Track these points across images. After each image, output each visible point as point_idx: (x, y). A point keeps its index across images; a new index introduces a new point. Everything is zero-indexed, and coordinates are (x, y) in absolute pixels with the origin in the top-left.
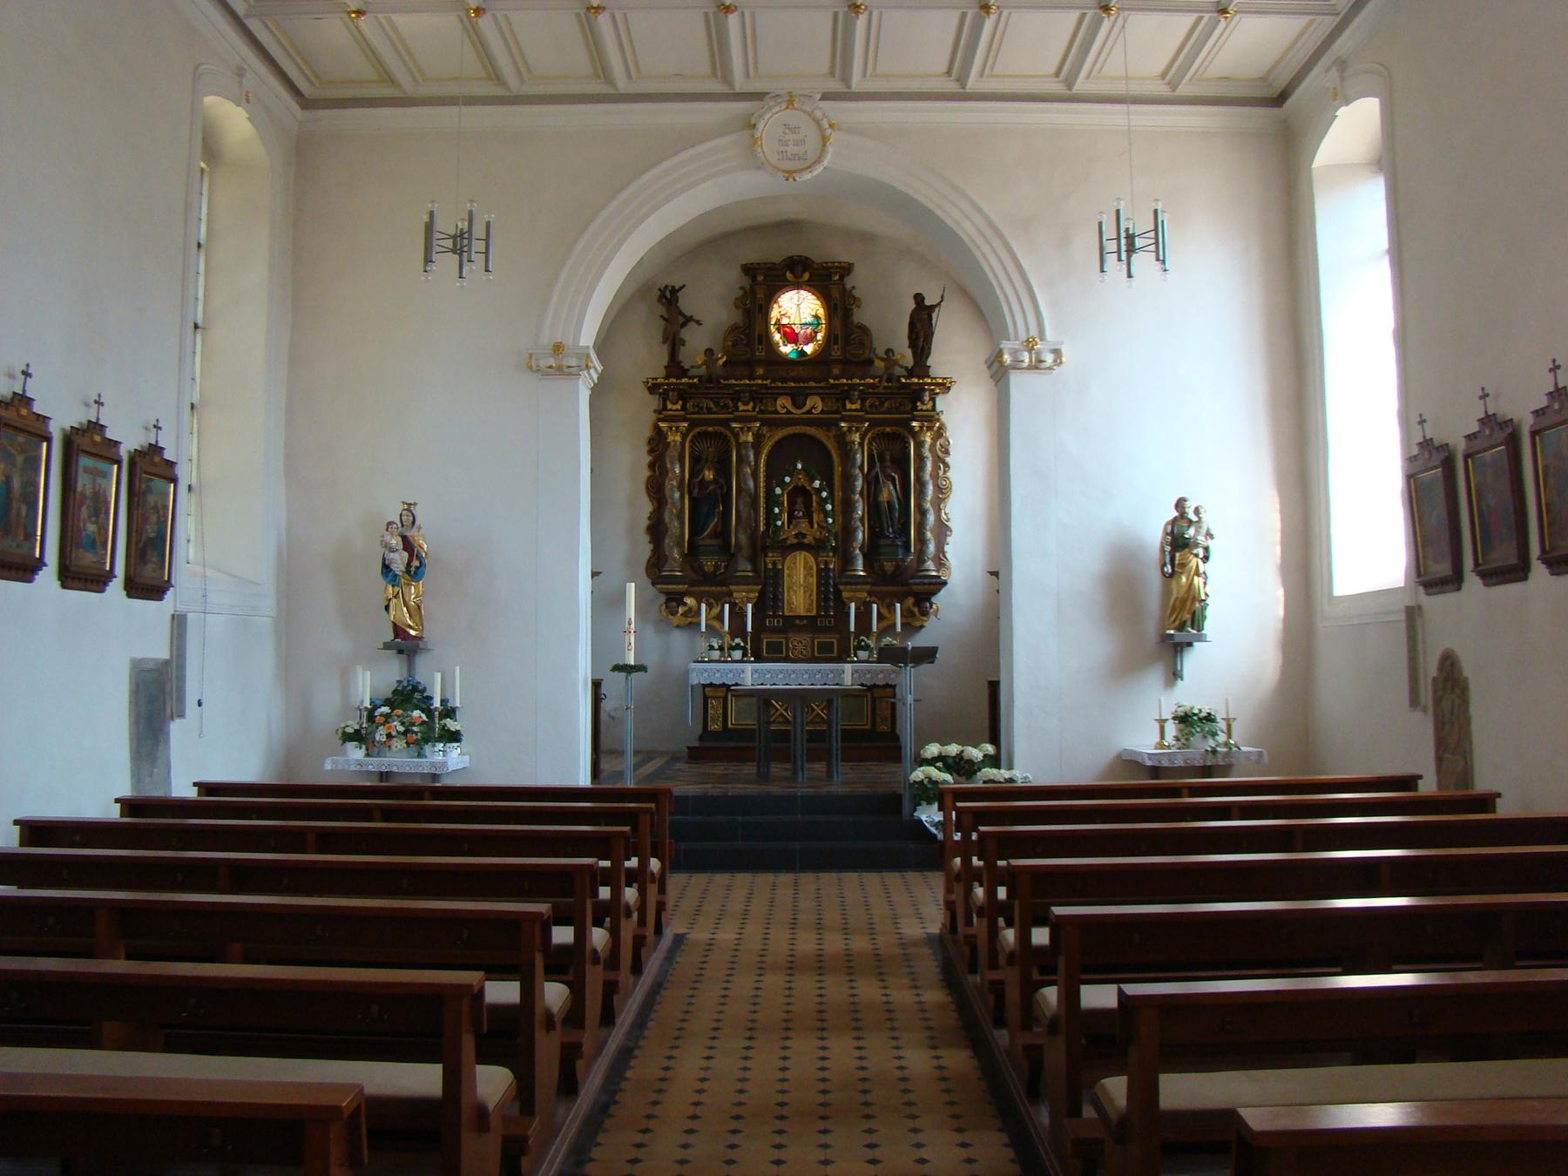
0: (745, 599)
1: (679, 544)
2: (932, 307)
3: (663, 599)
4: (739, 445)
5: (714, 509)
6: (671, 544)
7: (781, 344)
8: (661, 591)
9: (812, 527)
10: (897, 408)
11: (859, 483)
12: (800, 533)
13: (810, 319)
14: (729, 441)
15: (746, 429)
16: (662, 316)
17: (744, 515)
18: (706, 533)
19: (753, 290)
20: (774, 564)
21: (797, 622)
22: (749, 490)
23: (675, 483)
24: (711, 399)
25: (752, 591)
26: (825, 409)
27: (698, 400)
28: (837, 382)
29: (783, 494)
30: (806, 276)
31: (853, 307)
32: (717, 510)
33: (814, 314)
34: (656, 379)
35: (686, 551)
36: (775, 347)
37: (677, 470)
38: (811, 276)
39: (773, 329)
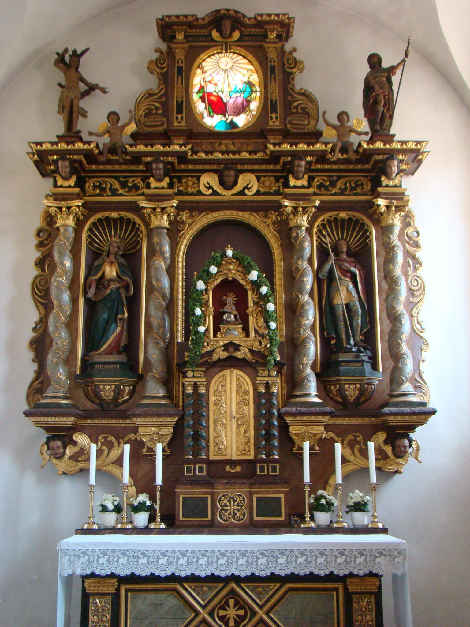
0: (155, 437)
1: (68, 361)
2: (392, 70)
3: (44, 436)
4: (150, 232)
5: (117, 314)
6: (55, 360)
7: (205, 115)
8: (38, 424)
9: (248, 335)
10: (352, 189)
11: (309, 281)
12: (231, 344)
13: (240, 86)
14: (138, 229)
15: (159, 210)
16: (59, 85)
17: (155, 322)
18: (105, 346)
19: (171, 53)
20: (196, 387)
21: (228, 468)
22: (162, 288)
23: (64, 280)
24: (117, 178)
25: (165, 425)
26: (262, 190)
27: (100, 180)
28: (278, 148)
29: (207, 290)
30: (236, 35)
31: (295, 70)
32: (120, 316)
33: (246, 80)
34: (40, 144)
35: (78, 372)
36: (198, 118)
37: (68, 263)
38: (242, 36)
39: (196, 97)
